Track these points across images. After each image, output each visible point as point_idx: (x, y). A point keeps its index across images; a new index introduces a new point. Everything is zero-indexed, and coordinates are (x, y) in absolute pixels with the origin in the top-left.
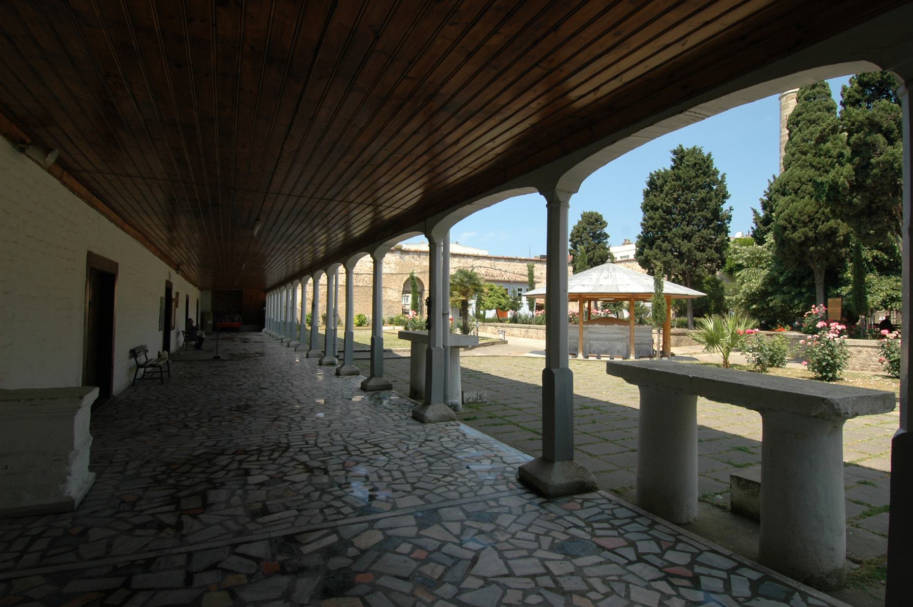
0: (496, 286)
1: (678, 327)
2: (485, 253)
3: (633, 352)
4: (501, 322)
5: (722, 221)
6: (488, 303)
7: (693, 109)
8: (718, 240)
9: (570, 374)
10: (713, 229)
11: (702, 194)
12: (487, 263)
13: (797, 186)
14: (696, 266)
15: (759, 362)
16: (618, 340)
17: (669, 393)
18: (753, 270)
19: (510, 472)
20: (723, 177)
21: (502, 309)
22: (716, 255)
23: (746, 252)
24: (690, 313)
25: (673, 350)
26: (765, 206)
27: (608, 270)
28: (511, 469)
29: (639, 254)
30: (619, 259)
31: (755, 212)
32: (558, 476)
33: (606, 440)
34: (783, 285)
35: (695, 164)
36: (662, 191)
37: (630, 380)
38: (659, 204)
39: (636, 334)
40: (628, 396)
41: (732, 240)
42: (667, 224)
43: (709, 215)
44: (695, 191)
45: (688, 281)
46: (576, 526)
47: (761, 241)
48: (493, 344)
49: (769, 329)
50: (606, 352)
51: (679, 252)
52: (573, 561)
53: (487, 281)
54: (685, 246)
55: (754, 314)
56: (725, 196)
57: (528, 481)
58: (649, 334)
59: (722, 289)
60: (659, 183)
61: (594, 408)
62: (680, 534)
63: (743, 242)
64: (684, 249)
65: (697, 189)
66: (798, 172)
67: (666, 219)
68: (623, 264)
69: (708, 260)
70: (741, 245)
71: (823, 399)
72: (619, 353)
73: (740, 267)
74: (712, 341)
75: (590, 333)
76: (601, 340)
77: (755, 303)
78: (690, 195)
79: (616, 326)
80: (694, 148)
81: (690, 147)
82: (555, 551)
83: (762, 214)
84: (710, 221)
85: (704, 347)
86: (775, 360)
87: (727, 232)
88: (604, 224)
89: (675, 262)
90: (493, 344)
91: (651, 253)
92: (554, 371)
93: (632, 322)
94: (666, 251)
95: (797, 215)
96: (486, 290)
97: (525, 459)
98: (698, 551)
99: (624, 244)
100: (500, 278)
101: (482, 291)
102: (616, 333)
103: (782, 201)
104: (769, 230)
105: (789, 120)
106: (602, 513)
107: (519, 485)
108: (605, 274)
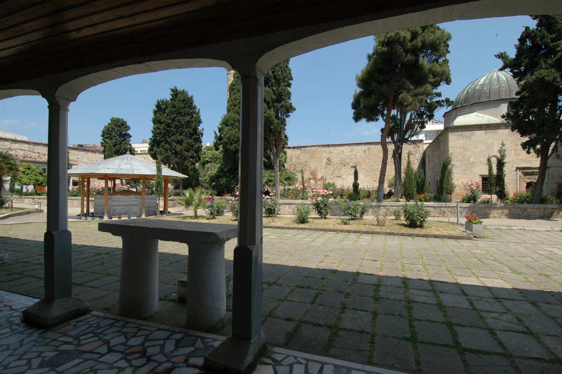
0: (33, 166)
1: (174, 196)
2: (25, 139)
3: (144, 212)
4: (39, 195)
5: (199, 135)
6: (25, 179)
7: (147, 63)
8: (196, 146)
9: (69, 234)
10: (194, 139)
11: (188, 118)
12: (26, 147)
13: (232, 122)
14: (185, 160)
15: (212, 214)
16: (134, 205)
17: (139, 240)
18: (213, 164)
19: (16, 317)
20: (199, 110)
21: (39, 185)
22: (195, 155)
23: (210, 154)
24: (181, 188)
25: (170, 210)
26: (220, 130)
27: (127, 159)
28: (18, 314)
29: (151, 150)
30: (139, 152)
31: (215, 133)
32: (57, 309)
33: (109, 275)
34: (227, 172)
35: (184, 100)
36: (164, 113)
37: (115, 234)
38: (163, 120)
39: (146, 201)
40: (117, 242)
41: (204, 147)
42: (167, 133)
43: (191, 131)
44: (184, 116)
45: (180, 168)
46: (66, 343)
47: (217, 149)
48: (29, 213)
49: (221, 196)
50: (125, 214)
51: (175, 151)
52: (57, 369)
53: (23, 161)
54: (179, 148)
55: (214, 188)
56: (200, 122)
57: (31, 320)
58: (155, 201)
59: (199, 173)
60: (163, 107)
61: (106, 254)
62: (142, 325)
63: (209, 149)
64: (178, 149)
65: (185, 115)
66: (233, 115)
67: (167, 130)
68: (141, 156)
69: (191, 157)
70: (208, 150)
71: (212, 233)
72: (134, 214)
73: (208, 162)
74: (188, 204)
75: (113, 201)
76: (122, 206)
77: (213, 182)
78: (181, 118)
79: (133, 196)
80: (183, 90)
81: (181, 89)
82: (43, 367)
83: (218, 135)
84: (192, 135)
85: (184, 207)
86: (219, 212)
87: (201, 142)
88: (128, 128)
89: (173, 157)
90: (29, 213)
91: (158, 150)
92: (54, 233)
93: (143, 194)
94: (167, 150)
95: (232, 137)
96: (21, 169)
97: (30, 302)
98: (150, 333)
99: (143, 143)
100: (38, 160)
101: (17, 170)
102: (132, 201)
103: (226, 129)
104: (221, 143)
105: (230, 87)
106: (91, 326)
107: (22, 325)
108: (125, 161)
